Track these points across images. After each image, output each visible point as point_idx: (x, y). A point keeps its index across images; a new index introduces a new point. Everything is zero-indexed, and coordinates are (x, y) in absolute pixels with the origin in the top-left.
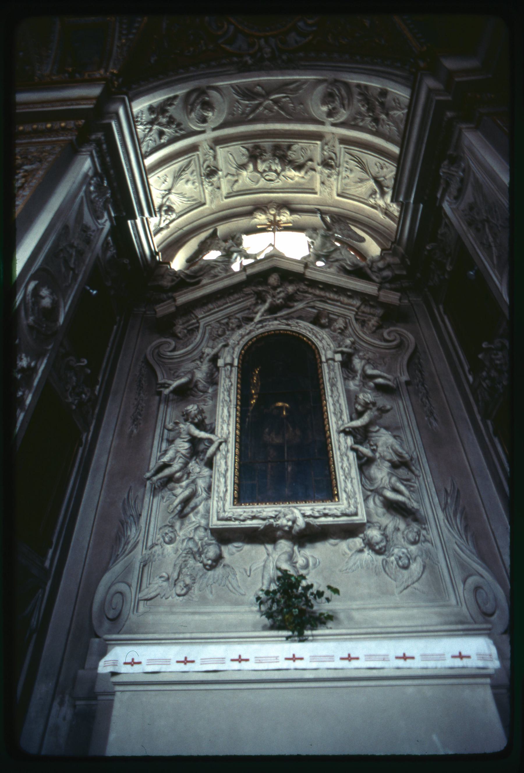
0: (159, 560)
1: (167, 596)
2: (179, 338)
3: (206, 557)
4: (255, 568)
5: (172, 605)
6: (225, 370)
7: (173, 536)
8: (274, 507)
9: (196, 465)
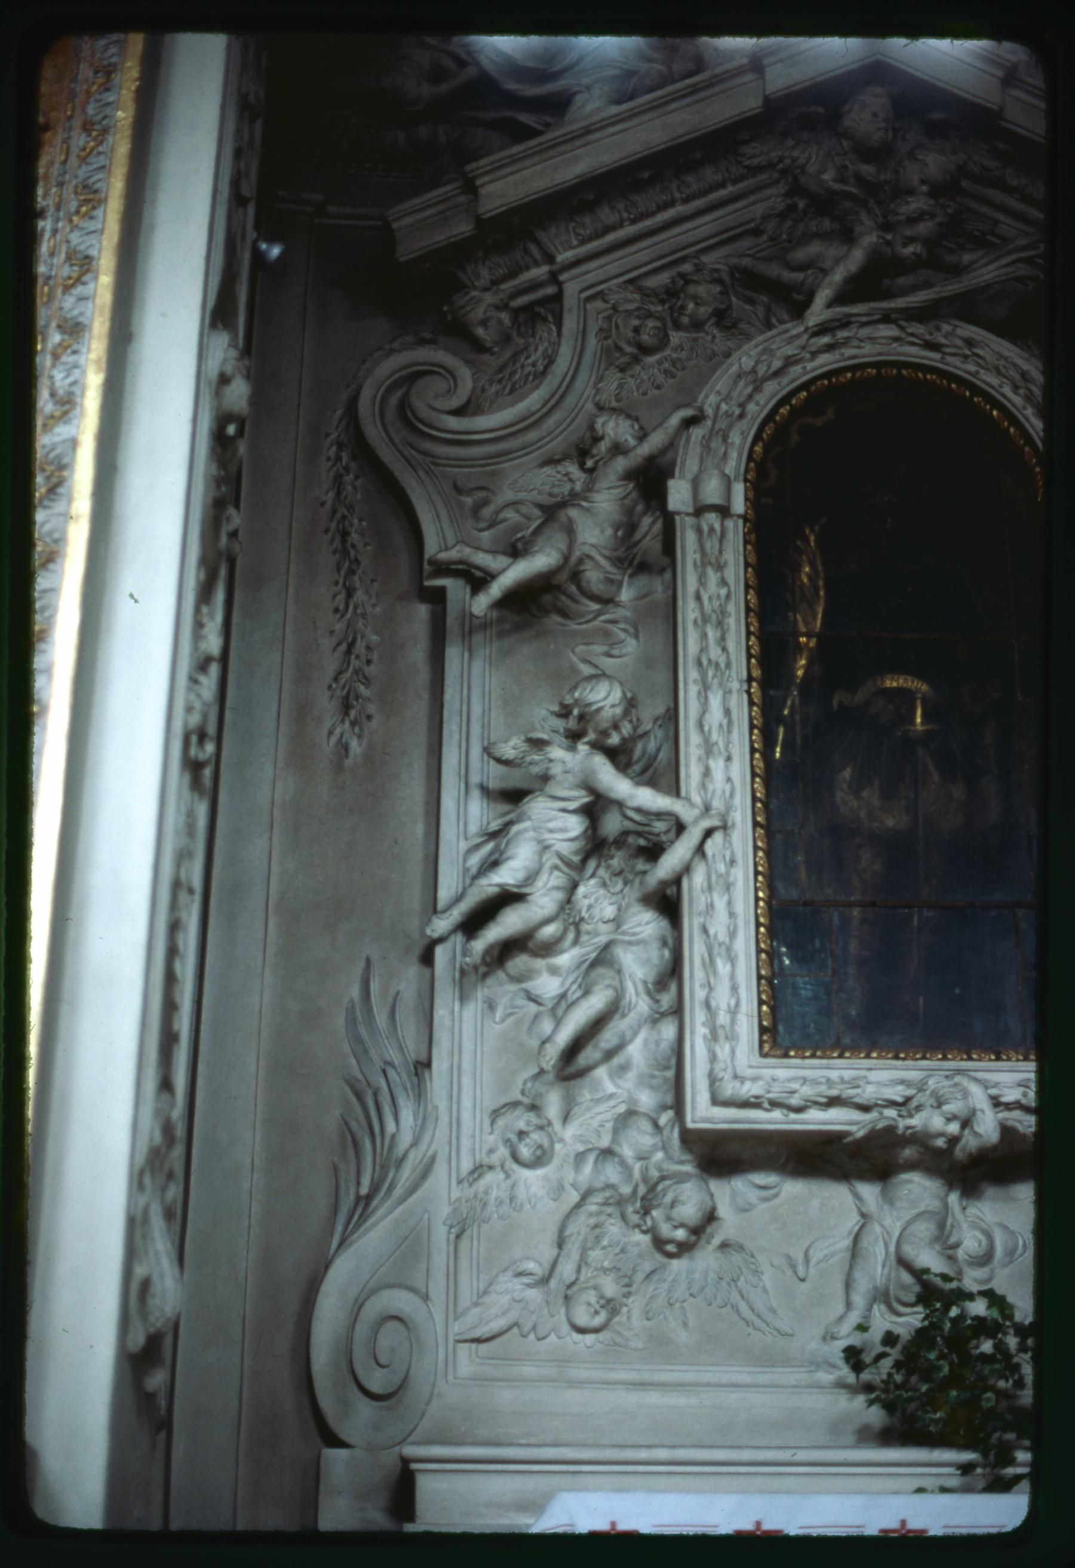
0: (501, 1218)
2: (479, 347)
3: (669, 1218)
4: (821, 1255)
5: (563, 1360)
6: (699, 530)
7: (546, 1143)
8: (896, 1068)
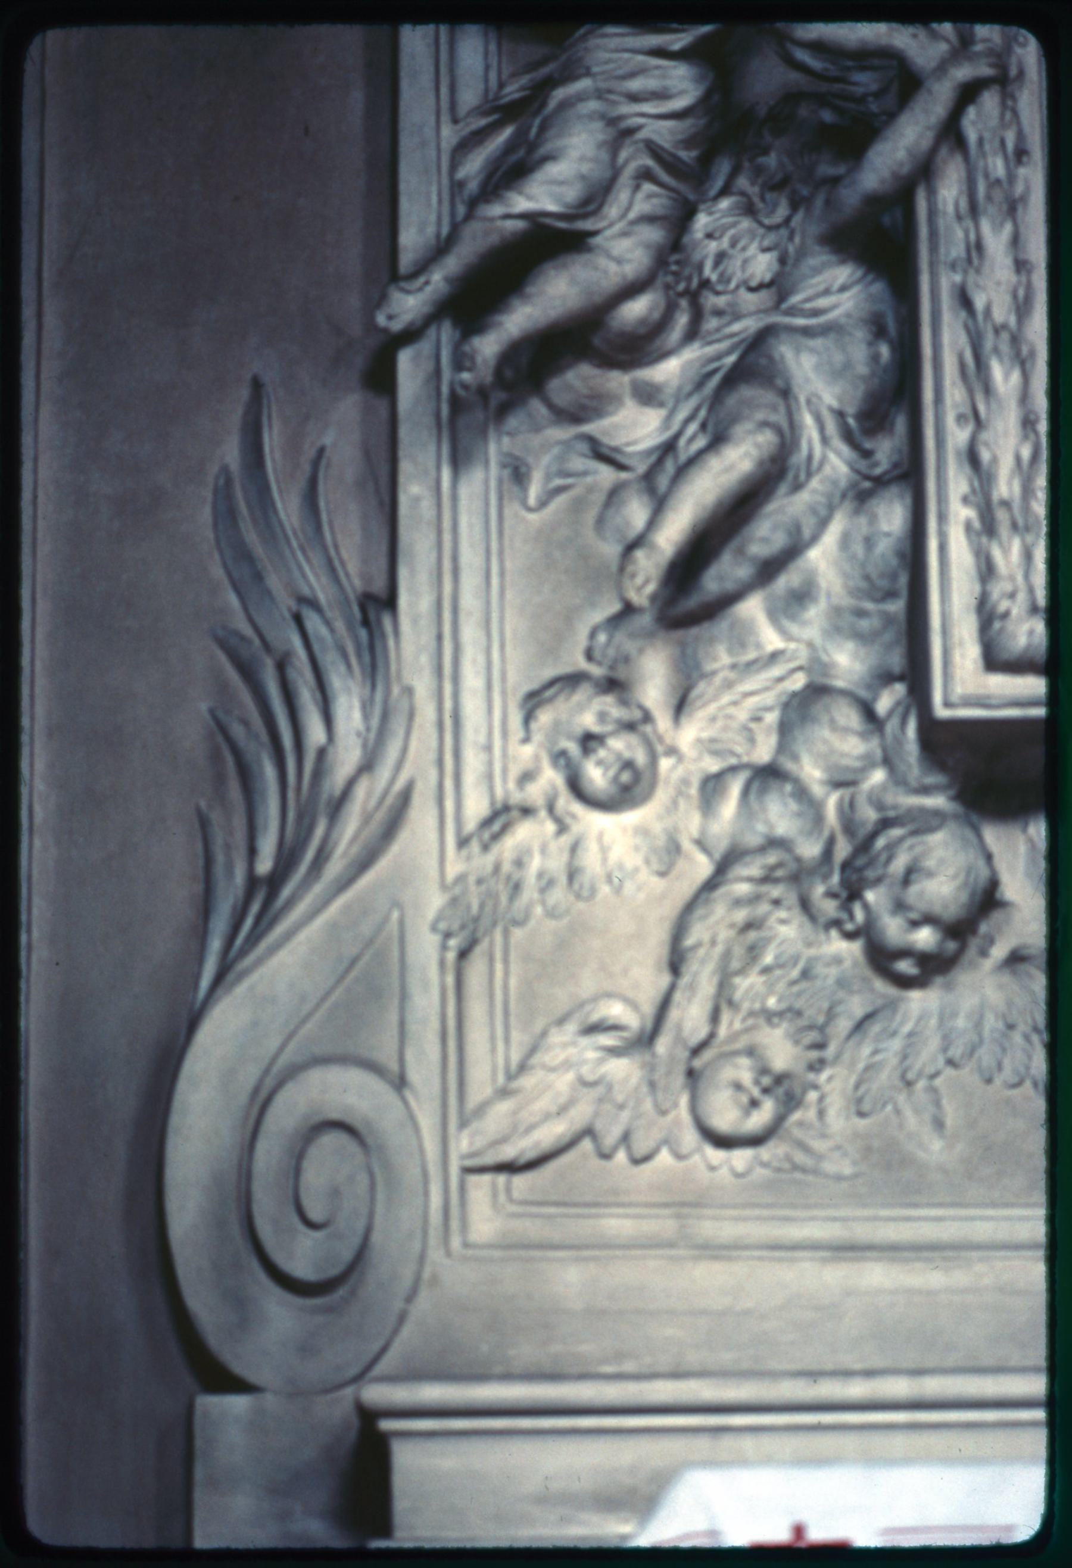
1: (641, 1147)
7: (641, 758)
9: (746, 223)
